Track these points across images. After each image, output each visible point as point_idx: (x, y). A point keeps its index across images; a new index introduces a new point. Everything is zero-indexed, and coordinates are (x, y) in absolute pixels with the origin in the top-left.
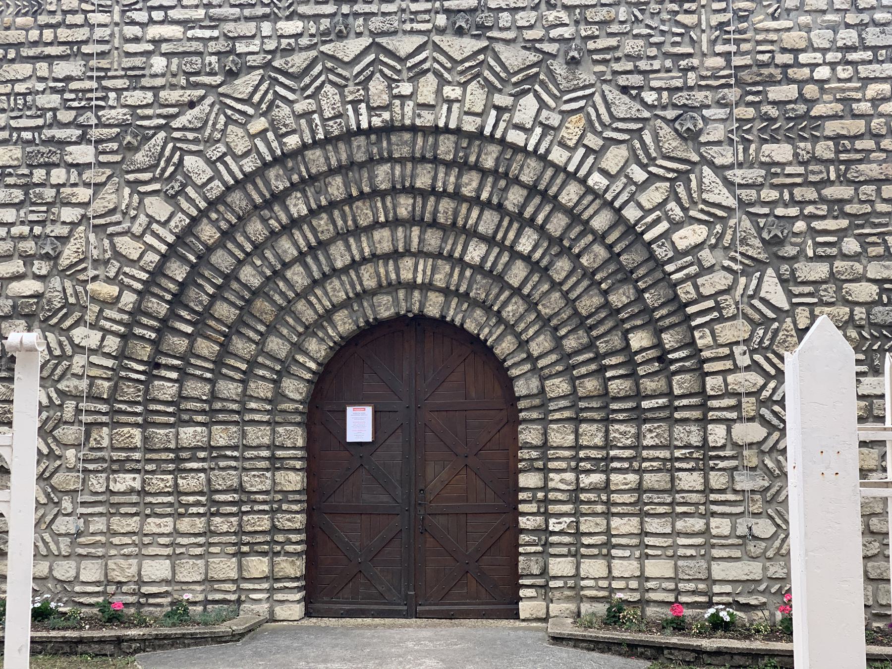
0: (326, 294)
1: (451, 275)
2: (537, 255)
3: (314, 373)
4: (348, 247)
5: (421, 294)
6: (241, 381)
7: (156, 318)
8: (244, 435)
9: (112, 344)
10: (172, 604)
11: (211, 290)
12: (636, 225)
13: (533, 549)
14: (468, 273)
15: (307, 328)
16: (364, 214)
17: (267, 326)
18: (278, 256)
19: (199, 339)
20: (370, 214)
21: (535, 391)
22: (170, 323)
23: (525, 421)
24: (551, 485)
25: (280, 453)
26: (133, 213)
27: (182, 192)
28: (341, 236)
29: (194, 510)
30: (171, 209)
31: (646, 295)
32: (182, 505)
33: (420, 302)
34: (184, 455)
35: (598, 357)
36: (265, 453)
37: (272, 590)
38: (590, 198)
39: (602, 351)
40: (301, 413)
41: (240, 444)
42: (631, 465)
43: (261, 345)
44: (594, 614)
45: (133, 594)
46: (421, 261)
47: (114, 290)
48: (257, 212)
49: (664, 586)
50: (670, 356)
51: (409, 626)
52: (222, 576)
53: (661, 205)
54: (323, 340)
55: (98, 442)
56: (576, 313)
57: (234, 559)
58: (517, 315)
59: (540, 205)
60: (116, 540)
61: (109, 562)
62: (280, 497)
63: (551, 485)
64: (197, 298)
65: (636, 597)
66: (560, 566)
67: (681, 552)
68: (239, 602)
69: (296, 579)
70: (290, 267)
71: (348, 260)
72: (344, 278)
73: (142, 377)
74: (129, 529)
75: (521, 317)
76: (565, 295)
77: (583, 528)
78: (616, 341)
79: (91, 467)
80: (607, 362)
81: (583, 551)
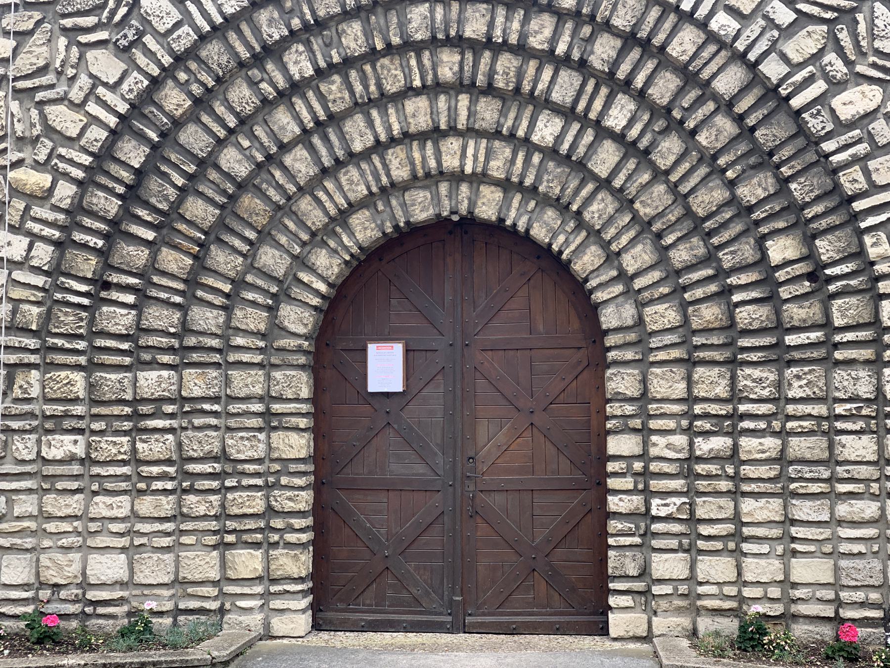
0: (340, 187)
1: (513, 162)
2: (634, 133)
3: (323, 297)
4: (370, 124)
5: (471, 188)
6: (224, 308)
7: (103, 219)
8: (228, 382)
9: (43, 254)
10: (129, 614)
11: (180, 181)
12: (779, 85)
13: (628, 541)
14: (536, 159)
15: (313, 234)
16: (392, 76)
17: (259, 232)
18: (272, 134)
19: (164, 250)
20: (401, 76)
21: (630, 322)
22: (123, 227)
23: (616, 363)
24: (653, 452)
25: (277, 407)
26: (70, 72)
27: (137, 42)
28: (360, 106)
29: (159, 485)
30: (123, 66)
31: (793, 186)
32: (142, 478)
33: (469, 199)
34: (145, 409)
35: (721, 274)
36: (258, 407)
37: (267, 596)
38: (712, 48)
39: (726, 265)
40: (306, 352)
41: (223, 394)
42: (769, 426)
43: (250, 257)
44: (717, 634)
45: (74, 602)
46: (471, 143)
47: (45, 179)
48: (243, 72)
49: (818, 594)
50: (828, 272)
51: (458, 649)
52: (198, 577)
53: (815, 58)
54: (335, 251)
55: (25, 391)
56: (689, 213)
57: (215, 553)
58: (605, 217)
59: (639, 60)
60: (51, 527)
61: (42, 557)
62: (276, 467)
63: (653, 452)
64: (160, 193)
65: (777, 609)
66: (669, 565)
67: (844, 548)
68: (222, 611)
69: (301, 580)
70: (290, 151)
71: (370, 141)
72: (364, 166)
73: (85, 301)
74: (69, 511)
75: (611, 220)
76: (673, 188)
77: (701, 513)
78: (747, 251)
79: (15, 425)
80: (733, 280)
81: (701, 544)
